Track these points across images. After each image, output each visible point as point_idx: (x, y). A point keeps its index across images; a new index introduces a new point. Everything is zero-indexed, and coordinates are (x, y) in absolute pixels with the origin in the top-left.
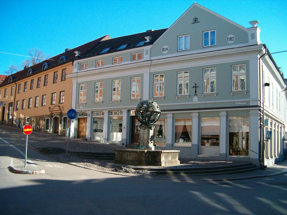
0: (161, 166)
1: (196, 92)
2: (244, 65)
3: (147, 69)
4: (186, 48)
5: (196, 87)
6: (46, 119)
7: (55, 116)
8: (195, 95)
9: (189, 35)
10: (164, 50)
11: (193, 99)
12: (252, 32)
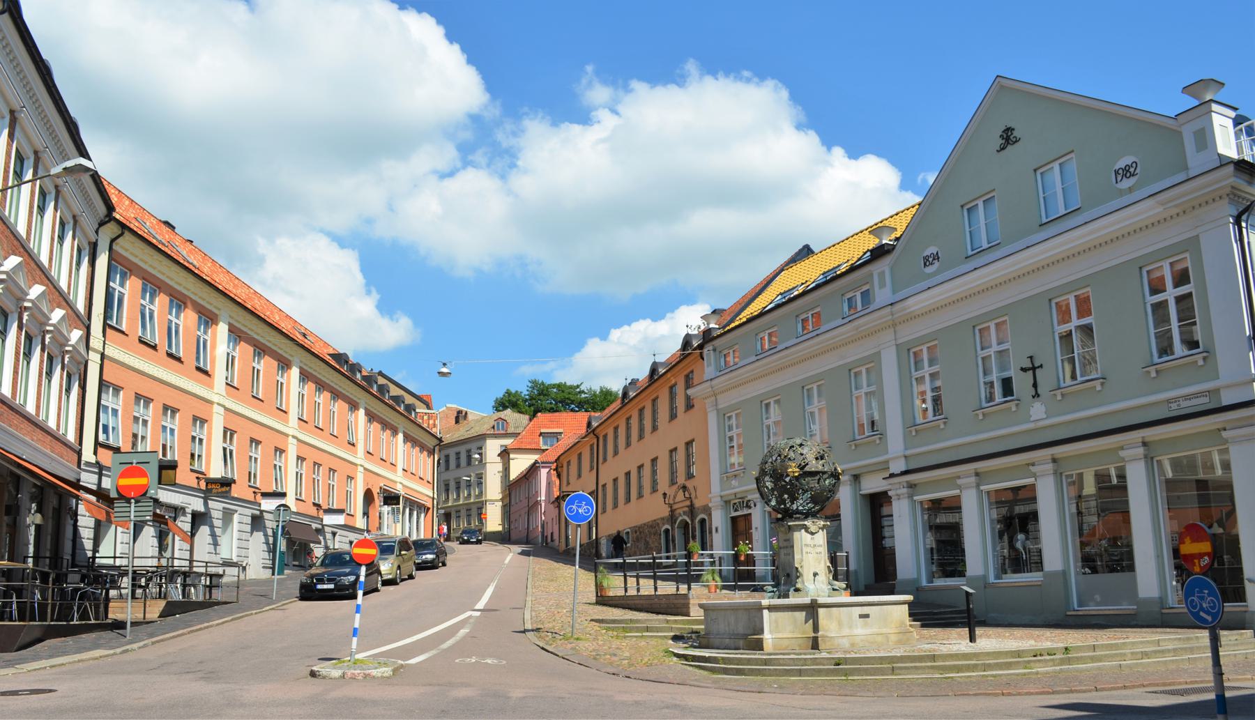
0: (763, 650)
1: (1035, 385)
2: (1004, 319)
3: (888, 336)
4: (975, 247)
5: (1034, 369)
6: (662, 530)
7: (680, 518)
8: (1033, 397)
9: (1072, 155)
10: (928, 264)
11: (1031, 413)
12: (1196, 125)
